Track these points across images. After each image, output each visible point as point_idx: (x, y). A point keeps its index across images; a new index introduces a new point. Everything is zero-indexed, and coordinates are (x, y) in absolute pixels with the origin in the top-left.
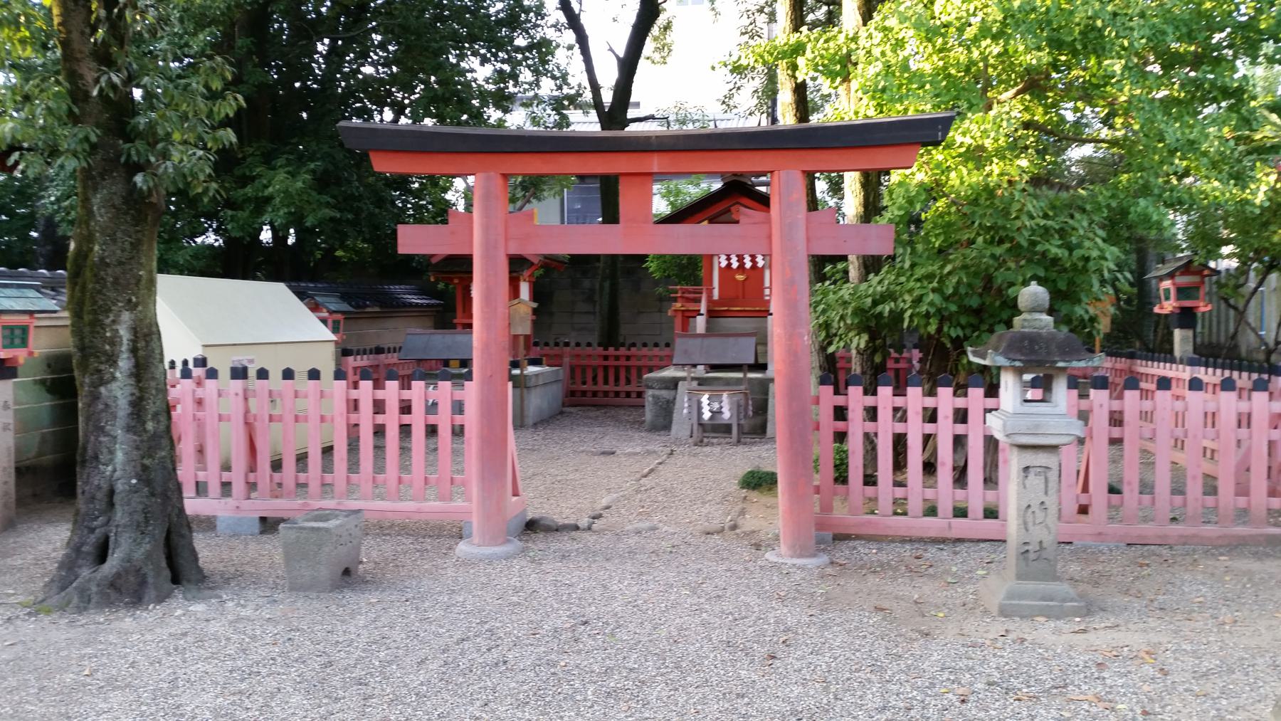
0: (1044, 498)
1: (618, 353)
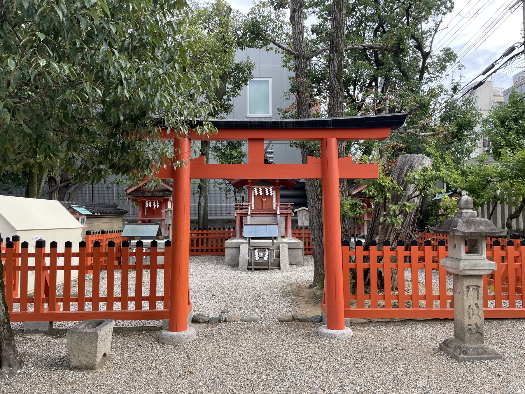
0: (476, 302)
1: (202, 232)
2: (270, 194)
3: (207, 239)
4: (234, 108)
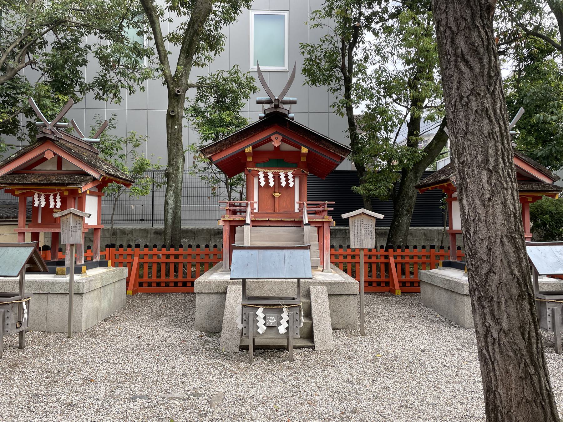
1: (177, 253)
2: (288, 184)
4: (227, 43)
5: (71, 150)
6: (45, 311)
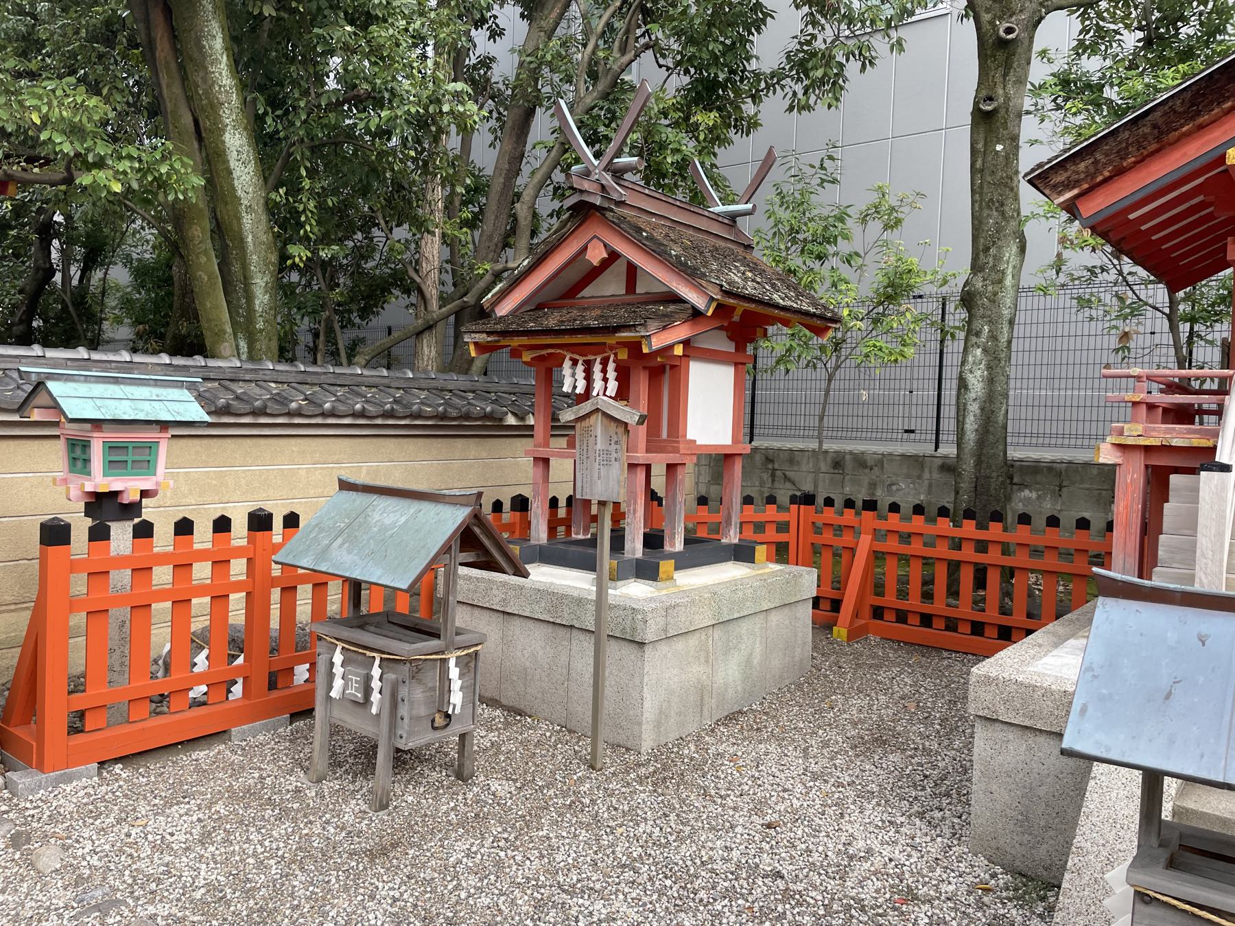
1: (958, 533)
3: (1009, 573)
5: (639, 230)
6: (565, 672)
